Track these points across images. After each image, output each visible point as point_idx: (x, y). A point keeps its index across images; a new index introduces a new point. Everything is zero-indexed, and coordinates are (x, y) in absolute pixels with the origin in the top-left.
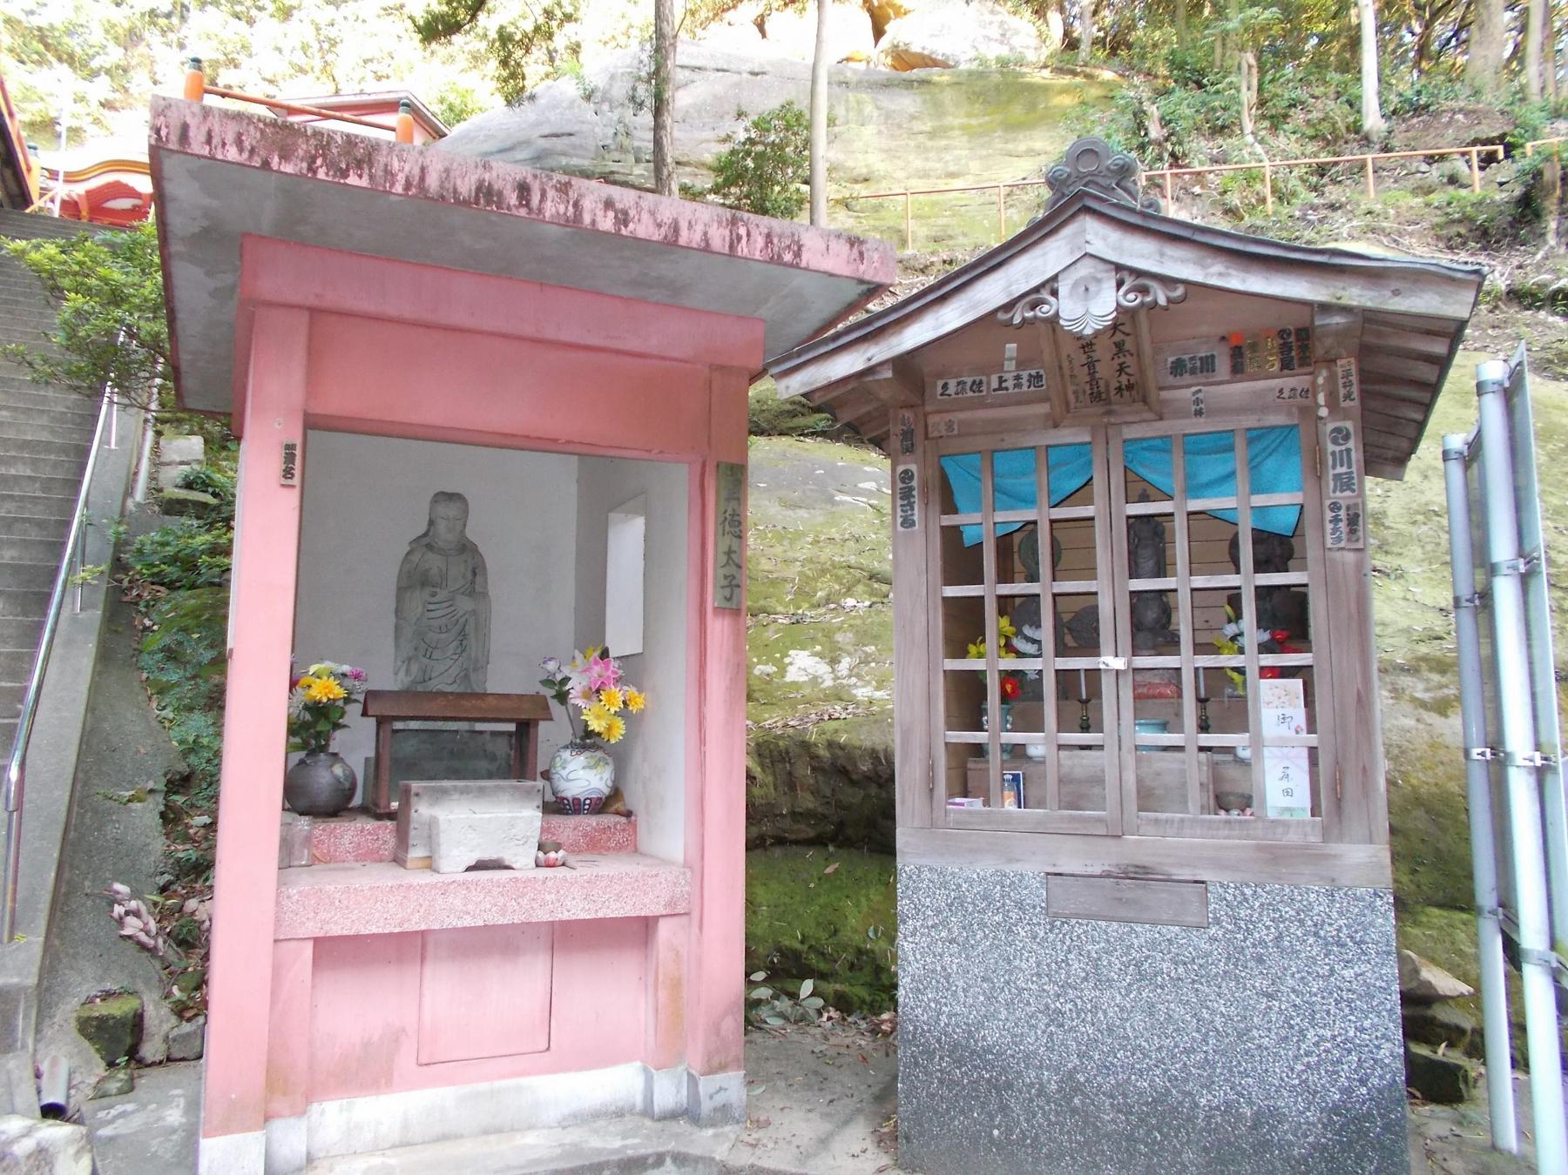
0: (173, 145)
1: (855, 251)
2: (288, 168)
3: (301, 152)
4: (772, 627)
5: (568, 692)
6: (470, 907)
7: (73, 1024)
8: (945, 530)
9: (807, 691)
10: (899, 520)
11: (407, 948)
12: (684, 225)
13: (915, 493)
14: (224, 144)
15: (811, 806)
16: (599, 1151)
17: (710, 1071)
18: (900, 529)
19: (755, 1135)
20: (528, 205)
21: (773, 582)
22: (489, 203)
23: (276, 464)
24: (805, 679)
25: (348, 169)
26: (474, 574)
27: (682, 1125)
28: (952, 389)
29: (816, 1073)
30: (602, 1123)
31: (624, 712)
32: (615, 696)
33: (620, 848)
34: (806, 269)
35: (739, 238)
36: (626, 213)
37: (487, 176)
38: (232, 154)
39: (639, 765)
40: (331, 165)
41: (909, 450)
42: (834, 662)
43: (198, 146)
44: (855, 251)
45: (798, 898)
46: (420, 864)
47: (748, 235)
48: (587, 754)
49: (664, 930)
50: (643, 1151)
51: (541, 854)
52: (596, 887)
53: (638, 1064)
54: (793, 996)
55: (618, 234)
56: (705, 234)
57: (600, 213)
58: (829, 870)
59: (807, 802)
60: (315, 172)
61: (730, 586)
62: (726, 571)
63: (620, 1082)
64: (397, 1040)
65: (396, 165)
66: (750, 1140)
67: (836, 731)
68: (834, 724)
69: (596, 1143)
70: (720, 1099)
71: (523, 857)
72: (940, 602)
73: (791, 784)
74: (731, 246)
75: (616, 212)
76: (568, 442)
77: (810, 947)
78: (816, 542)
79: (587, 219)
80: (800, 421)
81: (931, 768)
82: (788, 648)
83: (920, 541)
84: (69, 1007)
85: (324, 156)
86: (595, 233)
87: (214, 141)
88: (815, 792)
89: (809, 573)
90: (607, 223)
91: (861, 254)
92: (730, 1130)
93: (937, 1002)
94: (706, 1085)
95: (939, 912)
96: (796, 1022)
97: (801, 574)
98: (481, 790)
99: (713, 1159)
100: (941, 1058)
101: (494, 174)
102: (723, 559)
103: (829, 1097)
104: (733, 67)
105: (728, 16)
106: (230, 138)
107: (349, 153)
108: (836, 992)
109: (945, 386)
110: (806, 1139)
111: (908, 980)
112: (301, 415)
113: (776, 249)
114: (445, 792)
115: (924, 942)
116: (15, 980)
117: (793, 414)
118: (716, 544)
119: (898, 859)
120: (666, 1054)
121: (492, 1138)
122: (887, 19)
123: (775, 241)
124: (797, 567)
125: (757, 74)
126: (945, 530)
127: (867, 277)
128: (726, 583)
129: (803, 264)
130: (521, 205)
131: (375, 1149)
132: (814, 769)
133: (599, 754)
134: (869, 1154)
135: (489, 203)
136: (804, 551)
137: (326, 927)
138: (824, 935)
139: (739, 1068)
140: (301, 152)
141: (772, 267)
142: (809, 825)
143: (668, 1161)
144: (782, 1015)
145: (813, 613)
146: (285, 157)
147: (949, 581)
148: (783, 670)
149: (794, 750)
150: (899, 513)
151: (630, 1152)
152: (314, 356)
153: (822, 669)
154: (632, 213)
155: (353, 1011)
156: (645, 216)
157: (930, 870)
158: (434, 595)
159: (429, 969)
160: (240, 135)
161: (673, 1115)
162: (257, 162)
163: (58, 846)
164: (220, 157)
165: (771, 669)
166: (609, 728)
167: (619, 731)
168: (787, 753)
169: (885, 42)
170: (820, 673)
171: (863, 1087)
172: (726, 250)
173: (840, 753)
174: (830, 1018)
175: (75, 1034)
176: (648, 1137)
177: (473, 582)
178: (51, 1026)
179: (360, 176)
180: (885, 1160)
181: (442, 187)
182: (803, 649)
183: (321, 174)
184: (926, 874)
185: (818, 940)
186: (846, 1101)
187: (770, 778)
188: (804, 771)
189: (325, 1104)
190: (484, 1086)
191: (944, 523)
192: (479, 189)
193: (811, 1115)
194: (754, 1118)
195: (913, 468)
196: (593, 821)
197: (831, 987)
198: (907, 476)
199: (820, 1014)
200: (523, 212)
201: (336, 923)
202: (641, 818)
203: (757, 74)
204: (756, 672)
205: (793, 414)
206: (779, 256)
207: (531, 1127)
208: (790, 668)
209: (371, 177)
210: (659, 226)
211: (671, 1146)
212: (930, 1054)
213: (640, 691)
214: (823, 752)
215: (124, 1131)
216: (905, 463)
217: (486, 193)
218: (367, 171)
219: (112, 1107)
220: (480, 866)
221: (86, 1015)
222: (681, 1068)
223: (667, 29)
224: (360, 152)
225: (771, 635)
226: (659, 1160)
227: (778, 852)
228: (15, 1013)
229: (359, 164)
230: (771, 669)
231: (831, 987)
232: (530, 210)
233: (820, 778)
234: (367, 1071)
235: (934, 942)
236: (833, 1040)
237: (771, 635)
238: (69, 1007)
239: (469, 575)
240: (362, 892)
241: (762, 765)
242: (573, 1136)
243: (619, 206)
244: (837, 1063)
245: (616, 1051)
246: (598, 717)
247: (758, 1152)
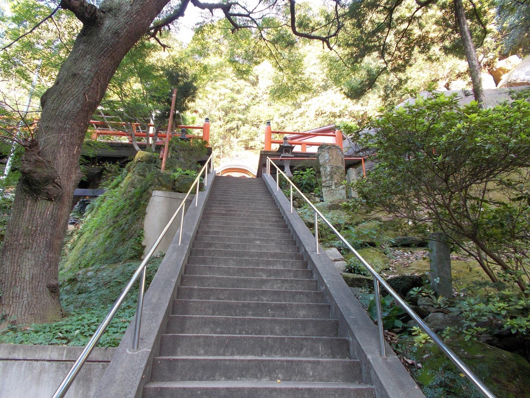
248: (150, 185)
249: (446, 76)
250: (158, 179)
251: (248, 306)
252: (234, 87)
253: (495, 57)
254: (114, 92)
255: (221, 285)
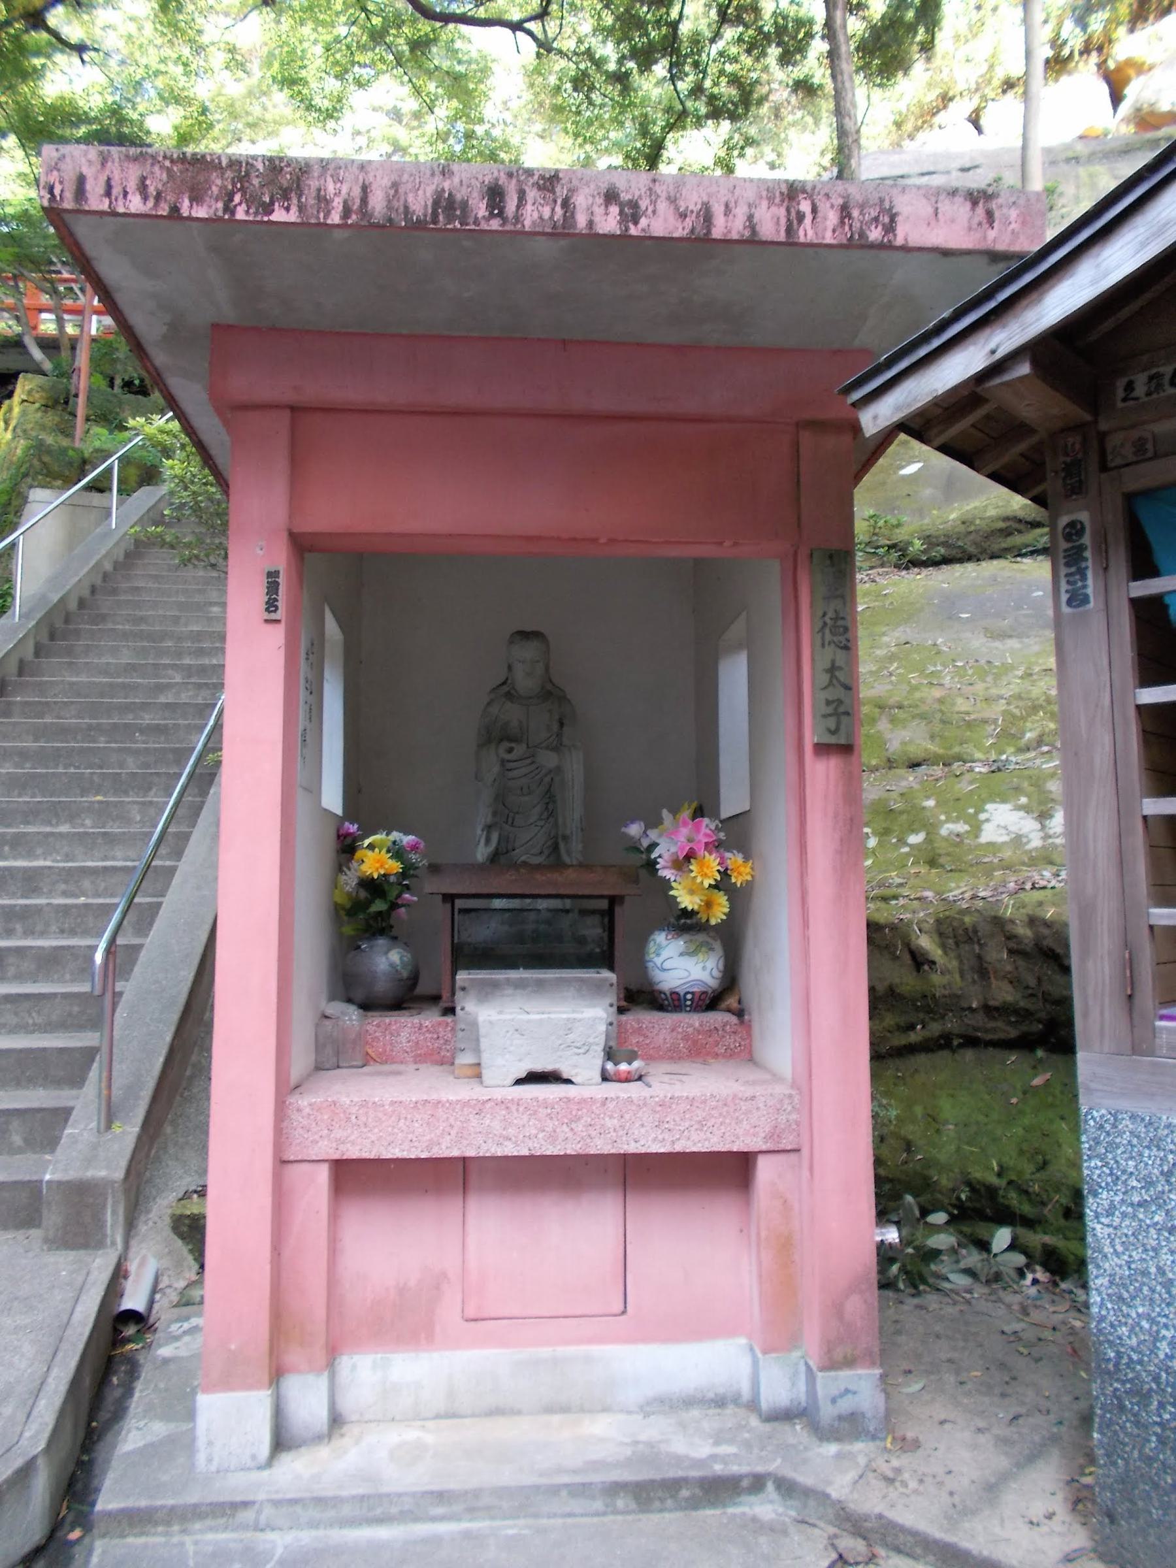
0: (68, 204)
1: (980, 210)
2: (201, 212)
3: (215, 189)
4: (968, 776)
5: (655, 862)
6: (511, 1131)
7: (168, 1220)
8: (1138, 605)
9: (1007, 854)
10: (1064, 597)
11: (447, 1178)
12: (718, 210)
13: (1088, 554)
14: (125, 194)
15: (1009, 998)
16: (679, 1460)
17: (831, 1365)
18: (1066, 609)
19: (895, 1463)
20: (501, 214)
21: (969, 725)
22: (450, 219)
23: (259, 596)
24: (1005, 838)
25: (272, 203)
26: (562, 724)
27: (798, 1433)
28: (1140, 390)
29: (1003, 1366)
30: (695, 1413)
31: (723, 883)
32: (709, 867)
33: (730, 1055)
34: (905, 249)
35: (801, 217)
36: (634, 205)
37: (446, 185)
38: (136, 204)
39: (752, 955)
40: (251, 200)
41: (1076, 489)
42: (1044, 816)
43: (96, 201)
44: (980, 210)
45: (995, 1116)
46: (469, 1072)
47: (814, 210)
48: (687, 937)
49: (765, 1171)
50: (735, 1469)
51: (610, 1066)
52: (682, 1105)
53: (743, 1341)
54: (984, 1246)
55: (625, 237)
56: (750, 217)
57: (599, 211)
58: (1037, 1081)
59: (1004, 993)
60: (233, 213)
61: (836, 714)
62: (831, 694)
63: (720, 1361)
64: (438, 1287)
65: (331, 188)
66: (886, 1469)
67: (1040, 904)
68: (1037, 895)
69: (680, 1446)
70: (845, 1405)
71: (584, 1068)
72: (1132, 713)
73: (982, 971)
74: (789, 230)
75: (622, 206)
76: (612, 541)
77: (1010, 1183)
78: (1028, 675)
79: (581, 221)
80: (1017, 540)
81: (1130, 965)
82: (984, 802)
83: (1098, 623)
84: (165, 1203)
85: (243, 190)
86: (594, 238)
87: (115, 192)
88: (1015, 981)
89: (1017, 712)
90: (609, 223)
91: (990, 215)
92: (860, 1448)
93: (1152, 1321)
94: (829, 1383)
95: (1149, 1183)
96: (988, 1282)
97: (1004, 713)
98: (540, 985)
99: (828, 1496)
100: (1161, 1405)
101: (456, 180)
102: (825, 678)
103: (1017, 1410)
104: (940, 167)
105: (937, 120)
106: (132, 185)
107: (271, 182)
108: (1045, 1245)
109: (1130, 387)
110: (966, 1481)
111: (1103, 1281)
112: (285, 535)
113: (856, 225)
114: (495, 985)
115: (1128, 1227)
116: (103, 1173)
117: (1006, 533)
118: (813, 660)
119: (1082, 1099)
120: (777, 1337)
121: (556, 1419)
122: (1126, 81)
123: (855, 213)
124: (1002, 706)
125: (968, 169)
126: (1138, 605)
127: (1001, 247)
128: (830, 710)
129: (899, 241)
130: (492, 216)
131: (416, 1417)
132: (1011, 952)
133: (701, 937)
134: (1056, 1525)
135: (450, 219)
136: (1013, 685)
137: (342, 1148)
138: (1029, 1168)
139: (873, 1364)
140: (215, 189)
141: (856, 254)
142: (1010, 1023)
143: (770, 1487)
144: (970, 1272)
145: (1020, 758)
146: (196, 199)
147: (1148, 679)
148: (977, 829)
149: (984, 929)
150: (1064, 586)
151: (718, 1468)
152: (296, 463)
153: (1028, 825)
154: (643, 204)
155: (389, 1248)
156: (662, 206)
157: (1133, 1117)
158: (510, 751)
159: (473, 1203)
160: (143, 179)
161: (784, 1415)
162: (164, 210)
163: (173, 1029)
164: (121, 210)
165: (962, 827)
166: (709, 904)
167: (721, 909)
168: (975, 932)
169: (1125, 108)
170: (1024, 831)
171: (1066, 1399)
172: (782, 237)
173: (1046, 932)
174: (1035, 1282)
175: (168, 1232)
176: (748, 1445)
177: (559, 735)
178: (146, 1222)
179: (288, 209)
180: (1080, 1539)
181: (389, 207)
182: (1004, 801)
183: (240, 215)
184: (1126, 1123)
185: (1020, 1173)
186: (1039, 1419)
187: (955, 963)
188: (997, 955)
189: (356, 1358)
190: (545, 1352)
191: (1133, 595)
192: (436, 203)
193: (982, 1439)
194: (899, 1434)
195: (1084, 517)
196: (695, 1020)
197: (1037, 1239)
198: (1074, 530)
199: (1021, 1273)
200: (495, 225)
201: (353, 1143)
202: (754, 1017)
203: (968, 169)
204: (944, 832)
205: (1006, 533)
206: (862, 235)
207: (606, 1409)
208: (986, 826)
209: (301, 208)
210: (683, 216)
211: (774, 1466)
212: (1145, 1397)
213: (747, 858)
214: (1023, 931)
215: (183, 1353)
216: (1069, 512)
217: (446, 204)
218: (295, 201)
219: (187, 1319)
220: (534, 1078)
221: (178, 1212)
222: (796, 1354)
223: (849, 124)
224: (285, 179)
225: (965, 786)
226: (757, 1483)
227: (969, 1055)
228: (104, 1206)
229: (285, 195)
230: (962, 827)
231: (1037, 1239)
232: (505, 221)
233: (1021, 963)
234: (406, 1322)
235: (1142, 1229)
236: (1036, 1316)
237: (965, 786)
238: (165, 1203)
239: (555, 727)
240: (396, 1106)
241: (943, 946)
242: (655, 1429)
243: (625, 197)
244: (1036, 1352)
245: (665, 1345)
246: (692, 892)
247: (893, 1494)
248: (26, 475)
249: (973, 86)
250: (40, 460)
251: (99, 728)
252: (399, 105)
253: (716, 36)
254: (410, 80)
255: (79, 695)
